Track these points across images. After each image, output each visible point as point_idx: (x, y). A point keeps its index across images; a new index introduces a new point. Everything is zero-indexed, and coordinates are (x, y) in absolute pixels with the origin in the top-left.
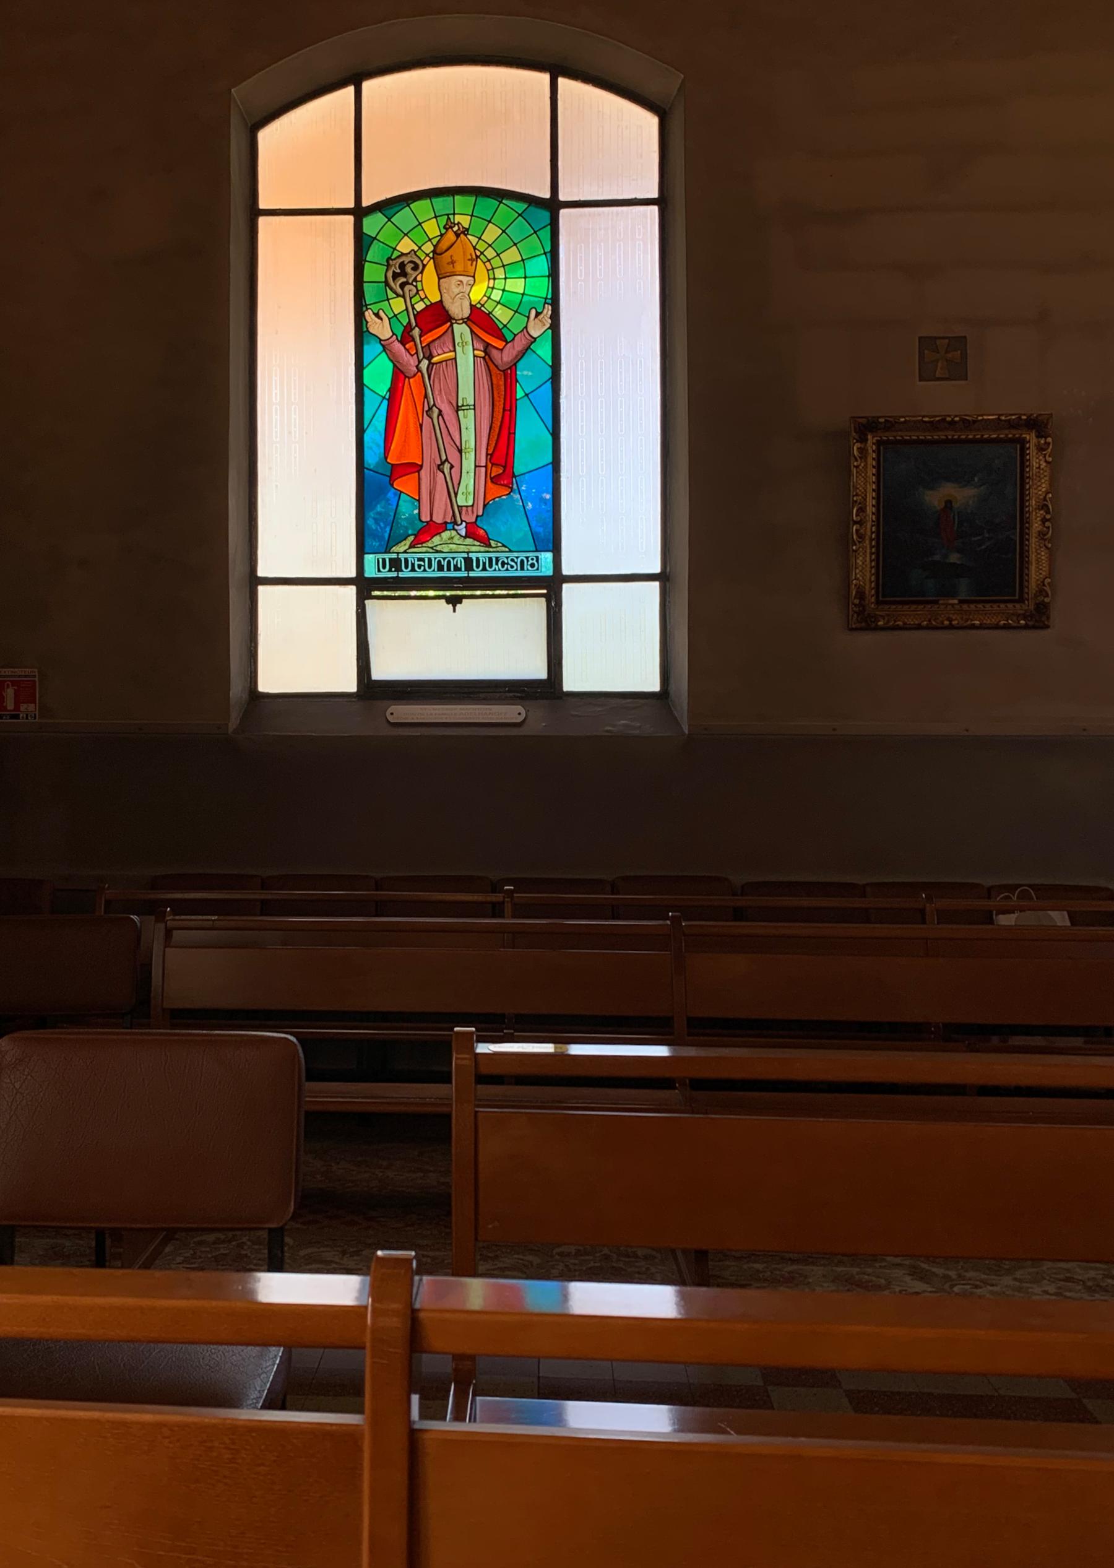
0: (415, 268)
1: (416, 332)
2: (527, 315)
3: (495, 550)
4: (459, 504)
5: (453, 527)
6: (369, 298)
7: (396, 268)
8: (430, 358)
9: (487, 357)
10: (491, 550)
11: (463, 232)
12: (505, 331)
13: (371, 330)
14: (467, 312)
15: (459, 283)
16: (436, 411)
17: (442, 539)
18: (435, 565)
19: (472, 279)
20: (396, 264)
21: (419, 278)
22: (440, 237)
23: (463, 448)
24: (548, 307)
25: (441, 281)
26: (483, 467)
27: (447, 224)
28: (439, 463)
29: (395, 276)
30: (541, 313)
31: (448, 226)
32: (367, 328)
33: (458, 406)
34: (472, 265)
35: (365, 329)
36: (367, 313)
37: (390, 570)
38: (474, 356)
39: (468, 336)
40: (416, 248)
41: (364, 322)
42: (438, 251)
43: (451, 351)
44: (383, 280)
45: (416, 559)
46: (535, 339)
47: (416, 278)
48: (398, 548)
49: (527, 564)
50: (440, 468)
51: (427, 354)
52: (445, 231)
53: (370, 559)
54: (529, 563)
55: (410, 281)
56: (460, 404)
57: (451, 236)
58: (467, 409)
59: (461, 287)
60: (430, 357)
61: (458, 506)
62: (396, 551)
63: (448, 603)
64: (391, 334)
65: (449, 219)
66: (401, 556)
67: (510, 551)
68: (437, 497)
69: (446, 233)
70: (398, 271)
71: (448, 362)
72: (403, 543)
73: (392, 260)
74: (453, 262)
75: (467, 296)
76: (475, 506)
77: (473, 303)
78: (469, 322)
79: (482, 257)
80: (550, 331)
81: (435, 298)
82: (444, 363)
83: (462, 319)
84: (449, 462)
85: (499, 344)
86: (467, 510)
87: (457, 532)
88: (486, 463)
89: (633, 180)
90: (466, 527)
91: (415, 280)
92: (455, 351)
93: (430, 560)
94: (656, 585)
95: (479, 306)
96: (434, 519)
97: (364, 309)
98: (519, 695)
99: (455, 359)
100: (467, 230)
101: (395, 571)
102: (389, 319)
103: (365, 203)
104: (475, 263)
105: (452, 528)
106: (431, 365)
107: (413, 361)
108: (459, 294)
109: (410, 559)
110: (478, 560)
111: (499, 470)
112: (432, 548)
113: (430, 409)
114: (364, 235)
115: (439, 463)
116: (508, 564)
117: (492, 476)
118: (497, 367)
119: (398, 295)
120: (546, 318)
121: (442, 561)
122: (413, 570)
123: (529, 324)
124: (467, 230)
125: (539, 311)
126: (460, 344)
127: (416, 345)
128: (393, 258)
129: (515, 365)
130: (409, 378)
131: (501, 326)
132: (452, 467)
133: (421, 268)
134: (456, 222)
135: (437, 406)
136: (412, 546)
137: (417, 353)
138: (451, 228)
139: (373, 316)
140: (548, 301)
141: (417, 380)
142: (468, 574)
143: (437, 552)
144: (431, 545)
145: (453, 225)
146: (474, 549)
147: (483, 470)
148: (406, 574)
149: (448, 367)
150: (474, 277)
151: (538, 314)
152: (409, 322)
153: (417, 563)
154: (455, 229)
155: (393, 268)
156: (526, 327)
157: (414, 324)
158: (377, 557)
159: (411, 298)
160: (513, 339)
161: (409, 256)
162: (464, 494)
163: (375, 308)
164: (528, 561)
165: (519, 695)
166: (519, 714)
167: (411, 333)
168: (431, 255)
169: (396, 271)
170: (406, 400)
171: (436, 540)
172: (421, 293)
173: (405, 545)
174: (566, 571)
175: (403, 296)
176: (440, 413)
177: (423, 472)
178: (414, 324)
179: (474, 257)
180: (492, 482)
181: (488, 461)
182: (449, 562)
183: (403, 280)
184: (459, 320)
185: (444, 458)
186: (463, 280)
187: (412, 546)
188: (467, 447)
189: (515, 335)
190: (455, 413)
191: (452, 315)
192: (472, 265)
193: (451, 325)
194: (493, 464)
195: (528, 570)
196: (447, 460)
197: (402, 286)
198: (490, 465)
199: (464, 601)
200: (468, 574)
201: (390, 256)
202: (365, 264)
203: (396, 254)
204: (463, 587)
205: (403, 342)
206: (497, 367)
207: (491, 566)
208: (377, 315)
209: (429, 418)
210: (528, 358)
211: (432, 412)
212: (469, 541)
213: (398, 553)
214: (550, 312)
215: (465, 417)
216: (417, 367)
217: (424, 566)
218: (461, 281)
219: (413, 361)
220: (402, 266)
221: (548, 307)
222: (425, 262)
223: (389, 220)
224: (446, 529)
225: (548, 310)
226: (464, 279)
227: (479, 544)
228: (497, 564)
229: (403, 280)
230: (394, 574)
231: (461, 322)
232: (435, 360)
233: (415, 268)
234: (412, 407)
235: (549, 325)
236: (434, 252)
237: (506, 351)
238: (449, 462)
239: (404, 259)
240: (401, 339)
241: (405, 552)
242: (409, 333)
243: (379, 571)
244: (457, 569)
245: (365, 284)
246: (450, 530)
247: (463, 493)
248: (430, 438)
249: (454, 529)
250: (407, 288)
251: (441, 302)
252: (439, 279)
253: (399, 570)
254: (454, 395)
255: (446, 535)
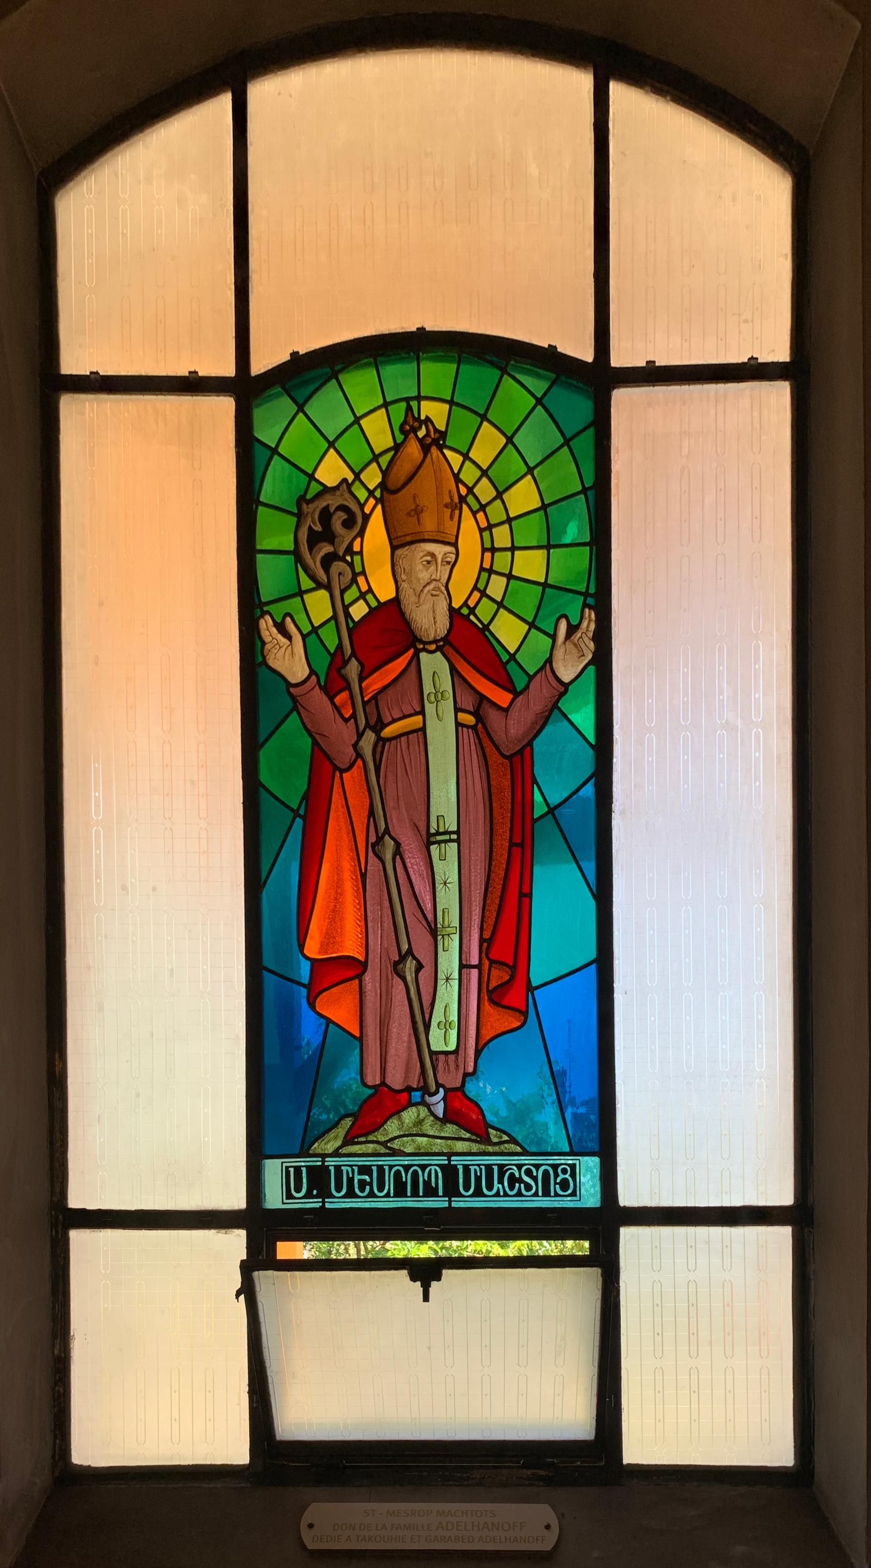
0: (349, 524)
1: (353, 669)
2: (552, 632)
3: (496, 1149)
4: (434, 1048)
5: (423, 1097)
6: (267, 588)
7: (314, 523)
8: (378, 728)
9: (480, 726)
10: (490, 1149)
11: (435, 442)
12: (512, 667)
13: (271, 663)
14: (441, 626)
15: (429, 558)
16: (389, 843)
17: (403, 1123)
18: (390, 1185)
19: (452, 549)
20: (314, 510)
21: (356, 547)
22: (391, 454)
23: (439, 926)
24: (590, 615)
25: (399, 552)
26: (474, 967)
27: (405, 422)
28: (397, 959)
29: (314, 539)
30: (577, 627)
31: (408, 428)
32: (264, 657)
33: (429, 835)
34: (452, 518)
35: (260, 659)
36: (262, 623)
37: (308, 1195)
38: (458, 724)
39: (446, 683)
40: (350, 477)
41: (259, 644)
42: (391, 485)
43: (416, 713)
44: (291, 547)
45: (356, 1169)
46: (566, 686)
47: (350, 546)
48: (322, 1145)
49: (556, 1183)
50: (397, 968)
51: (373, 722)
52: (403, 437)
53: (273, 1170)
54: (558, 1180)
55: (341, 553)
56: (432, 831)
57: (413, 449)
58: (445, 841)
59: (433, 568)
60: (378, 726)
61: (432, 1053)
62: (320, 1151)
63: (413, 1278)
64: (307, 671)
65: (409, 409)
66: (331, 1162)
67: (525, 1153)
68: (394, 1030)
69: (404, 440)
70: (318, 528)
71: (411, 736)
72: (332, 1134)
73: (309, 502)
74: (417, 512)
75: (443, 589)
76: (461, 1052)
77: (456, 605)
78: (447, 648)
79: (470, 499)
80: (592, 669)
81: (385, 591)
82: (404, 739)
83: (435, 641)
84: (415, 958)
85: (502, 698)
86: (447, 1061)
87: (430, 1110)
88: (480, 959)
89: (746, 321)
90: (444, 1099)
91: (349, 550)
92: (422, 712)
93: (380, 1169)
94: (784, 1234)
95: (465, 611)
96: (389, 1081)
97: (258, 612)
98: (542, 1473)
99: (423, 729)
100: (443, 435)
101: (316, 1197)
102: (304, 637)
103: (259, 365)
104: (457, 512)
105: (419, 1100)
106: (380, 744)
107: (347, 732)
108: (428, 584)
109: (472, 1168)
110: (466, 1169)
111: (499, 976)
112: (384, 1144)
113: (380, 839)
114: (257, 445)
115: (397, 959)
116: (520, 1181)
117: (490, 988)
118: (497, 748)
119: (319, 585)
120: (586, 639)
121: (420, 1173)
122: (351, 1194)
123: (555, 652)
124: (443, 435)
125: (574, 622)
126: (432, 698)
127: (352, 697)
128: (309, 496)
129: (530, 744)
130: (342, 771)
131: (505, 657)
132: (419, 967)
133: (360, 520)
134: (423, 417)
135: (393, 834)
136: (348, 1140)
137: (354, 716)
138: (415, 430)
139: (274, 630)
140: (590, 601)
141: (355, 775)
142: (450, 1202)
143: (394, 1153)
144: (382, 1139)
145: (416, 424)
146: (460, 1146)
147: (475, 973)
148: (338, 1202)
149: (411, 747)
150: (455, 545)
151: (572, 630)
152: (340, 646)
153: (357, 1178)
154: (421, 433)
155: (309, 521)
156: (549, 661)
157: (348, 650)
158: (285, 1165)
159: (343, 592)
160: (527, 687)
161: (338, 493)
162: (442, 1026)
163: (278, 610)
164: (556, 1175)
165: (542, 1473)
166: (548, 1527)
167: (343, 671)
168: (378, 494)
169: (316, 528)
170: (337, 869)
171: (392, 1128)
172: (361, 580)
173: (336, 1137)
174: (627, 1198)
175: (328, 588)
176: (398, 851)
177: (367, 977)
178: (348, 650)
179: (456, 500)
180: (492, 1001)
181: (484, 955)
182: (415, 1175)
183: (327, 549)
184: (430, 643)
185: (405, 947)
186: (437, 553)
187: (348, 1140)
188: (446, 923)
189: (531, 678)
190: (424, 849)
191: (417, 633)
192: (452, 518)
193: (416, 656)
194: (492, 962)
195: (556, 1195)
196: (410, 951)
197: (327, 562)
198: (486, 963)
199: (445, 1272)
200: (450, 1202)
201: (302, 493)
202: (257, 508)
203: (314, 488)
204: (442, 1231)
205: (330, 691)
206: (497, 748)
207: (490, 1187)
208: (281, 628)
209: (377, 860)
210: (555, 730)
211: (384, 845)
212: (450, 1130)
213: (324, 1156)
214: (593, 626)
215: (443, 858)
216: (355, 746)
217: (371, 1184)
218: (433, 555)
219: (347, 732)
220: (326, 516)
221: (590, 615)
222: (367, 510)
223: (301, 408)
224: (410, 1104)
225: (590, 621)
226: (439, 550)
227: (468, 1135)
228: (501, 1181)
229: (327, 549)
230: (314, 1204)
231: (433, 647)
232: (388, 731)
233: (349, 524)
234: (348, 833)
235: (590, 656)
236: (382, 485)
237: (514, 713)
238: (415, 958)
239: (330, 502)
240: (325, 682)
241: (336, 1154)
242: (339, 670)
243: (289, 1196)
244: (431, 1191)
245: (259, 557)
246: (416, 1104)
247: (439, 1024)
248: (381, 904)
249: (423, 1103)
250: (337, 567)
251: (396, 602)
252: (394, 548)
253: (325, 1194)
254: (422, 808)
255: (409, 1115)
